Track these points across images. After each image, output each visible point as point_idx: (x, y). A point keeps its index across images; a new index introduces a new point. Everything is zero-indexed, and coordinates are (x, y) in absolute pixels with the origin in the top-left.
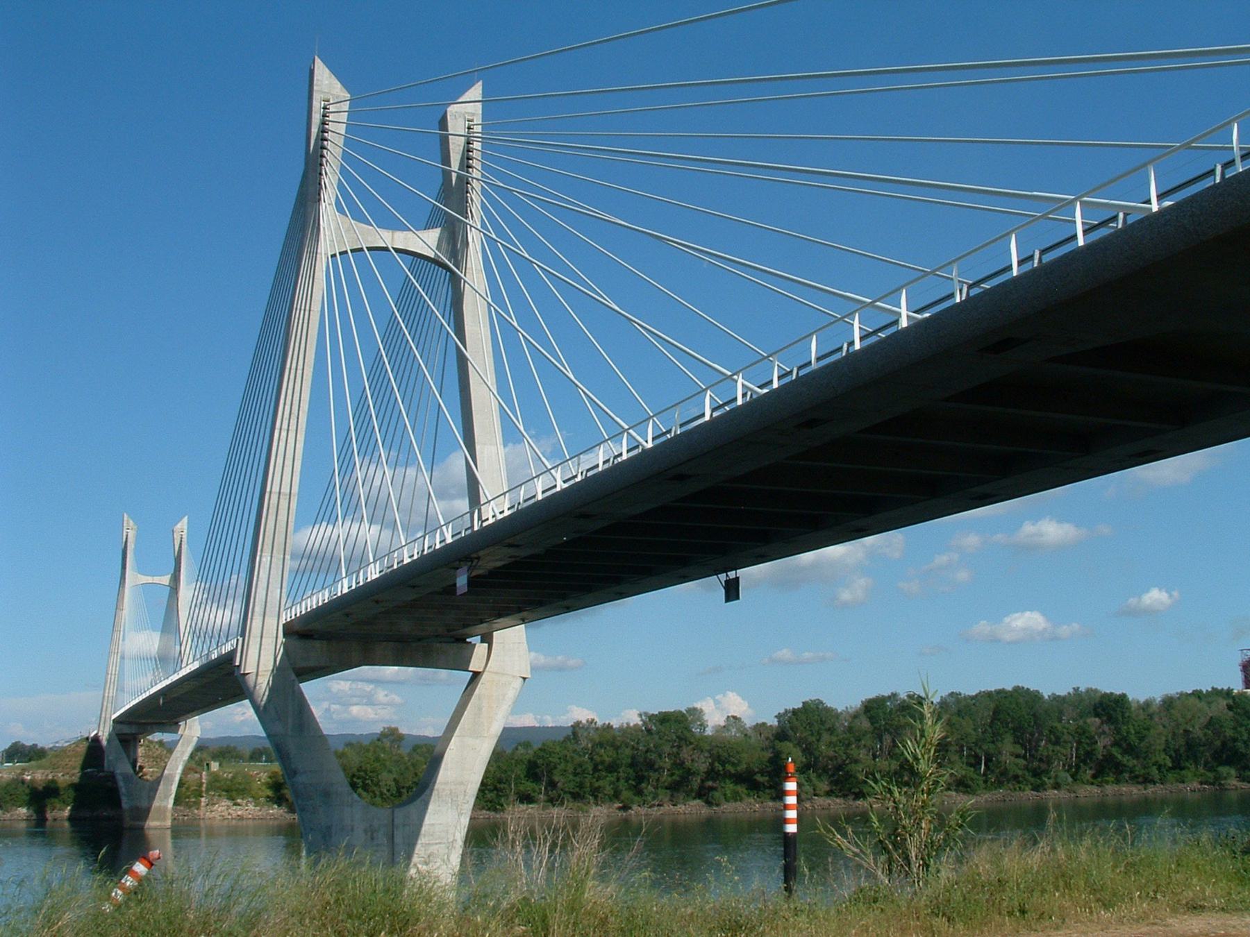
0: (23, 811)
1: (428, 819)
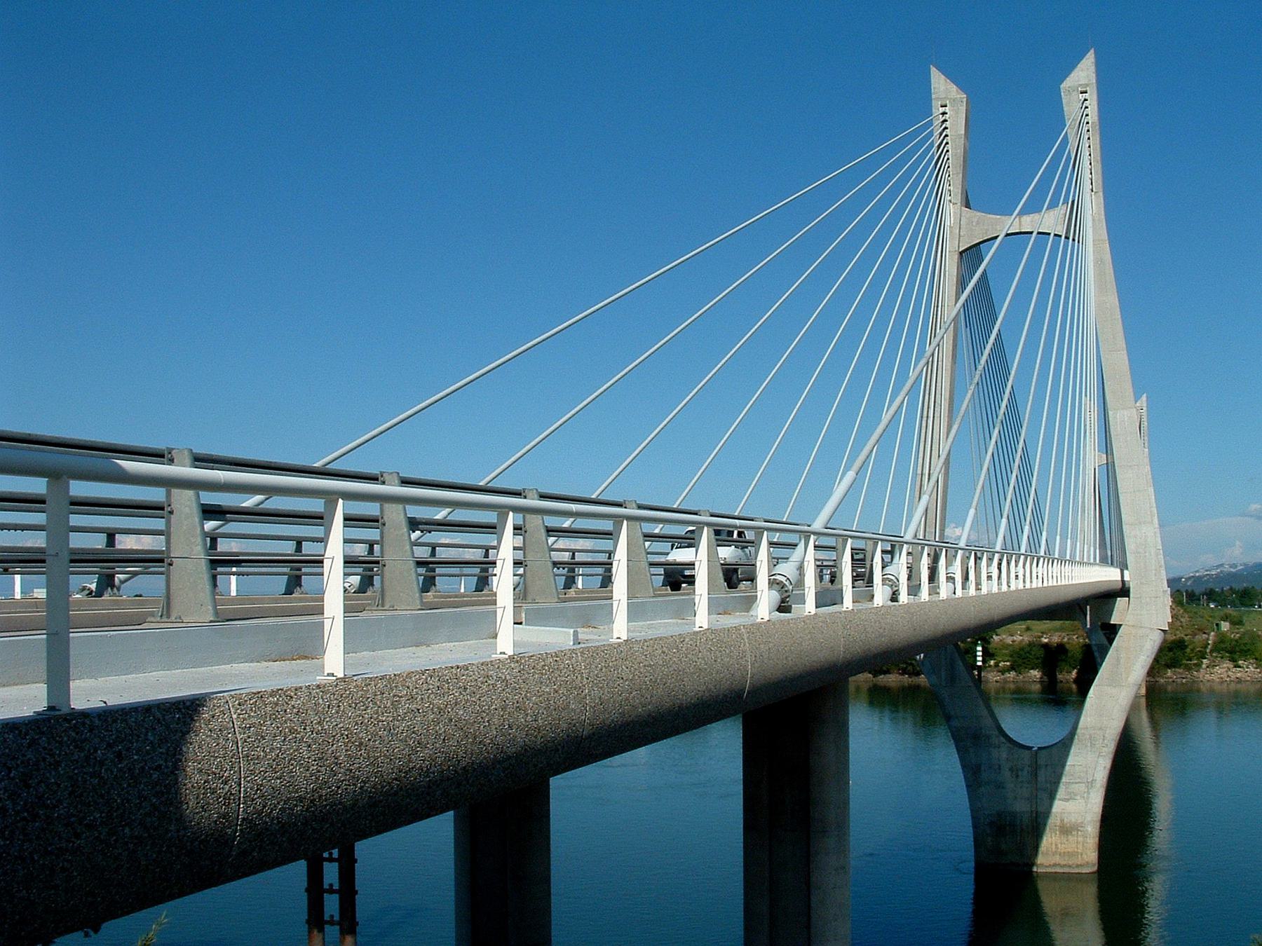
0: (1036, 674)
1: (1070, 761)
